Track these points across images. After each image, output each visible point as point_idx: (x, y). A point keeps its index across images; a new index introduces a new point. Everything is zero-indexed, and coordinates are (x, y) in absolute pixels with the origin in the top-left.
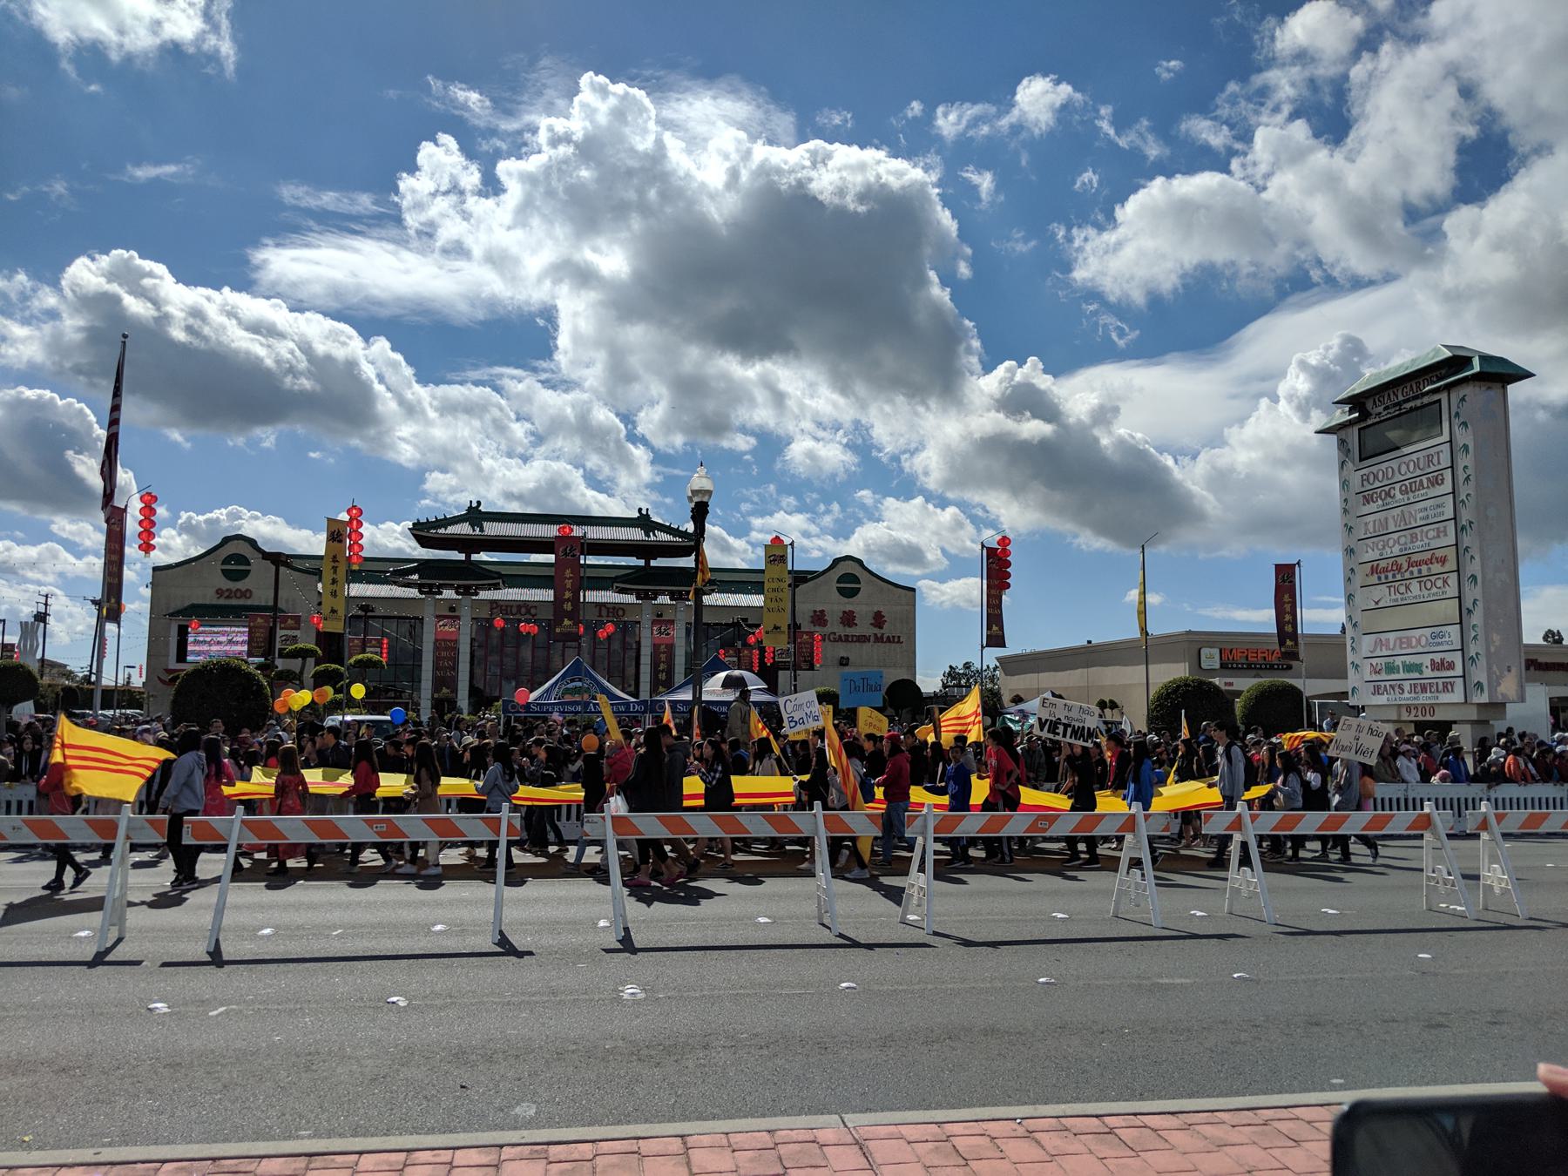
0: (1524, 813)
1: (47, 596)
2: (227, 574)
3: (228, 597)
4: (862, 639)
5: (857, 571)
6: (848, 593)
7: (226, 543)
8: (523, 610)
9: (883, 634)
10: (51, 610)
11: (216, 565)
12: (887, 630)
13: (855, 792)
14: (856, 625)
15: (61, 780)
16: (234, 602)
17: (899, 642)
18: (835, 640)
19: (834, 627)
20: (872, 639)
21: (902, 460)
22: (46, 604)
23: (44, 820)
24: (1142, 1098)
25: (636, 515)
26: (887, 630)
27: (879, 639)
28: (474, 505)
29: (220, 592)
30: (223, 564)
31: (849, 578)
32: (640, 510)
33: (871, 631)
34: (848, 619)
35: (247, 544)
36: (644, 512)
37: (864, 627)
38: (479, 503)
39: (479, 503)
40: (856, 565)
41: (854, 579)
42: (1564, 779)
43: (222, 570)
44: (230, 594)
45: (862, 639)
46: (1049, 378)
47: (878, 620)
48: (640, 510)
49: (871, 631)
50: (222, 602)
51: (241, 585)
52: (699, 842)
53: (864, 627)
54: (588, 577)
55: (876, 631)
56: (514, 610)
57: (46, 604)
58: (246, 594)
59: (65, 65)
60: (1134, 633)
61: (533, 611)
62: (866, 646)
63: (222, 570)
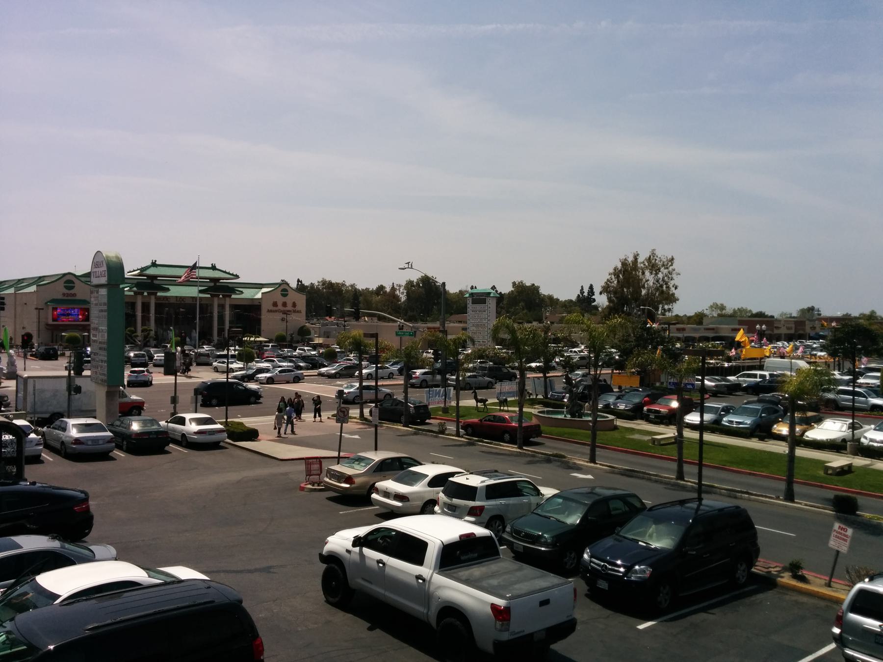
0: (64, 307)
2: (66, 287)
3: (67, 296)
5: (287, 287)
6: (285, 295)
8: (165, 299)
11: (61, 283)
13: (280, 367)
15: (788, 486)
16: (69, 298)
19: (280, 307)
21: (794, 329)
23: (820, 511)
25: (211, 266)
27: (295, 311)
28: (154, 261)
29: (64, 294)
31: (285, 290)
34: (285, 304)
35: (73, 276)
37: (289, 307)
39: (156, 261)
42: (882, 411)
43: (64, 286)
44: (68, 295)
48: (212, 264)
50: (65, 298)
51: (72, 292)
54: (197, 286)
55: (293, 308)
56: (162, 299)
58: (74, 295)
61: (169, 300)
63: (64, 286)
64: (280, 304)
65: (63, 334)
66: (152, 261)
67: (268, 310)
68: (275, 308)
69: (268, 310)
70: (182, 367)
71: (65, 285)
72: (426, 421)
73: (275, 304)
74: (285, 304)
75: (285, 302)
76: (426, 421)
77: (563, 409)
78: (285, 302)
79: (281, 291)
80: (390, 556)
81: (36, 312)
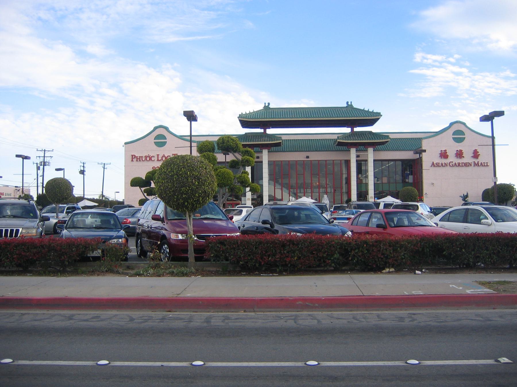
1: (84, 163)
4: (466, 165)
7: (156, 129)
9: (478, 162)
10: (85, 169)
12: (481, 160)
14: (464, 157)
17: (487, 166)
18: (453, 166)
19: (452, 158)
20: (473, 165)
22: (84, 167)
24: (361, 298)
25: (345, 105)
26: (481, 160)
27: (477, 165)
28: (267, 105)
30: (154, 139)
32: (347, 103)
33: (471, 160)
34: (459, 154)
36: (349, 103)
38: (269, 104)
39: (269, 104)
40: (463, 126)
41: (461, 132)
45: (466, 165)
46: (249, 174)
47: (476, 155)
48: (347, 103)
49: (471, 160)
52: (222, 236)
53: (468, 158)
57: (84, 167)
59: (160, 240)
60: (382, 190)
62: (469, 169)
63: (154, 142)
64: (451, 154)
65: (446, 261)
66: (265, 103)
67: (433, 163)
68: (444, 161)
69: (433, 163)
70: (101, 245)
71: (156, 141)
72: (151, 181)
73: (444, 155)
74: (459, 154)
75: (461, 151)
76: (151, 181)
77: (33, 205)
78: (461, 151)
79: (453, 134)
80: (357, 195)
81: (80, 167)
